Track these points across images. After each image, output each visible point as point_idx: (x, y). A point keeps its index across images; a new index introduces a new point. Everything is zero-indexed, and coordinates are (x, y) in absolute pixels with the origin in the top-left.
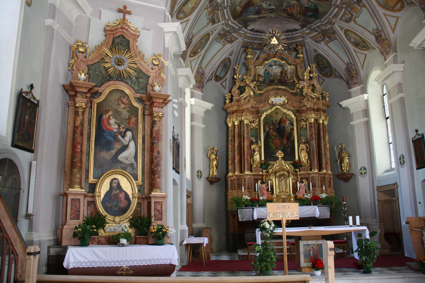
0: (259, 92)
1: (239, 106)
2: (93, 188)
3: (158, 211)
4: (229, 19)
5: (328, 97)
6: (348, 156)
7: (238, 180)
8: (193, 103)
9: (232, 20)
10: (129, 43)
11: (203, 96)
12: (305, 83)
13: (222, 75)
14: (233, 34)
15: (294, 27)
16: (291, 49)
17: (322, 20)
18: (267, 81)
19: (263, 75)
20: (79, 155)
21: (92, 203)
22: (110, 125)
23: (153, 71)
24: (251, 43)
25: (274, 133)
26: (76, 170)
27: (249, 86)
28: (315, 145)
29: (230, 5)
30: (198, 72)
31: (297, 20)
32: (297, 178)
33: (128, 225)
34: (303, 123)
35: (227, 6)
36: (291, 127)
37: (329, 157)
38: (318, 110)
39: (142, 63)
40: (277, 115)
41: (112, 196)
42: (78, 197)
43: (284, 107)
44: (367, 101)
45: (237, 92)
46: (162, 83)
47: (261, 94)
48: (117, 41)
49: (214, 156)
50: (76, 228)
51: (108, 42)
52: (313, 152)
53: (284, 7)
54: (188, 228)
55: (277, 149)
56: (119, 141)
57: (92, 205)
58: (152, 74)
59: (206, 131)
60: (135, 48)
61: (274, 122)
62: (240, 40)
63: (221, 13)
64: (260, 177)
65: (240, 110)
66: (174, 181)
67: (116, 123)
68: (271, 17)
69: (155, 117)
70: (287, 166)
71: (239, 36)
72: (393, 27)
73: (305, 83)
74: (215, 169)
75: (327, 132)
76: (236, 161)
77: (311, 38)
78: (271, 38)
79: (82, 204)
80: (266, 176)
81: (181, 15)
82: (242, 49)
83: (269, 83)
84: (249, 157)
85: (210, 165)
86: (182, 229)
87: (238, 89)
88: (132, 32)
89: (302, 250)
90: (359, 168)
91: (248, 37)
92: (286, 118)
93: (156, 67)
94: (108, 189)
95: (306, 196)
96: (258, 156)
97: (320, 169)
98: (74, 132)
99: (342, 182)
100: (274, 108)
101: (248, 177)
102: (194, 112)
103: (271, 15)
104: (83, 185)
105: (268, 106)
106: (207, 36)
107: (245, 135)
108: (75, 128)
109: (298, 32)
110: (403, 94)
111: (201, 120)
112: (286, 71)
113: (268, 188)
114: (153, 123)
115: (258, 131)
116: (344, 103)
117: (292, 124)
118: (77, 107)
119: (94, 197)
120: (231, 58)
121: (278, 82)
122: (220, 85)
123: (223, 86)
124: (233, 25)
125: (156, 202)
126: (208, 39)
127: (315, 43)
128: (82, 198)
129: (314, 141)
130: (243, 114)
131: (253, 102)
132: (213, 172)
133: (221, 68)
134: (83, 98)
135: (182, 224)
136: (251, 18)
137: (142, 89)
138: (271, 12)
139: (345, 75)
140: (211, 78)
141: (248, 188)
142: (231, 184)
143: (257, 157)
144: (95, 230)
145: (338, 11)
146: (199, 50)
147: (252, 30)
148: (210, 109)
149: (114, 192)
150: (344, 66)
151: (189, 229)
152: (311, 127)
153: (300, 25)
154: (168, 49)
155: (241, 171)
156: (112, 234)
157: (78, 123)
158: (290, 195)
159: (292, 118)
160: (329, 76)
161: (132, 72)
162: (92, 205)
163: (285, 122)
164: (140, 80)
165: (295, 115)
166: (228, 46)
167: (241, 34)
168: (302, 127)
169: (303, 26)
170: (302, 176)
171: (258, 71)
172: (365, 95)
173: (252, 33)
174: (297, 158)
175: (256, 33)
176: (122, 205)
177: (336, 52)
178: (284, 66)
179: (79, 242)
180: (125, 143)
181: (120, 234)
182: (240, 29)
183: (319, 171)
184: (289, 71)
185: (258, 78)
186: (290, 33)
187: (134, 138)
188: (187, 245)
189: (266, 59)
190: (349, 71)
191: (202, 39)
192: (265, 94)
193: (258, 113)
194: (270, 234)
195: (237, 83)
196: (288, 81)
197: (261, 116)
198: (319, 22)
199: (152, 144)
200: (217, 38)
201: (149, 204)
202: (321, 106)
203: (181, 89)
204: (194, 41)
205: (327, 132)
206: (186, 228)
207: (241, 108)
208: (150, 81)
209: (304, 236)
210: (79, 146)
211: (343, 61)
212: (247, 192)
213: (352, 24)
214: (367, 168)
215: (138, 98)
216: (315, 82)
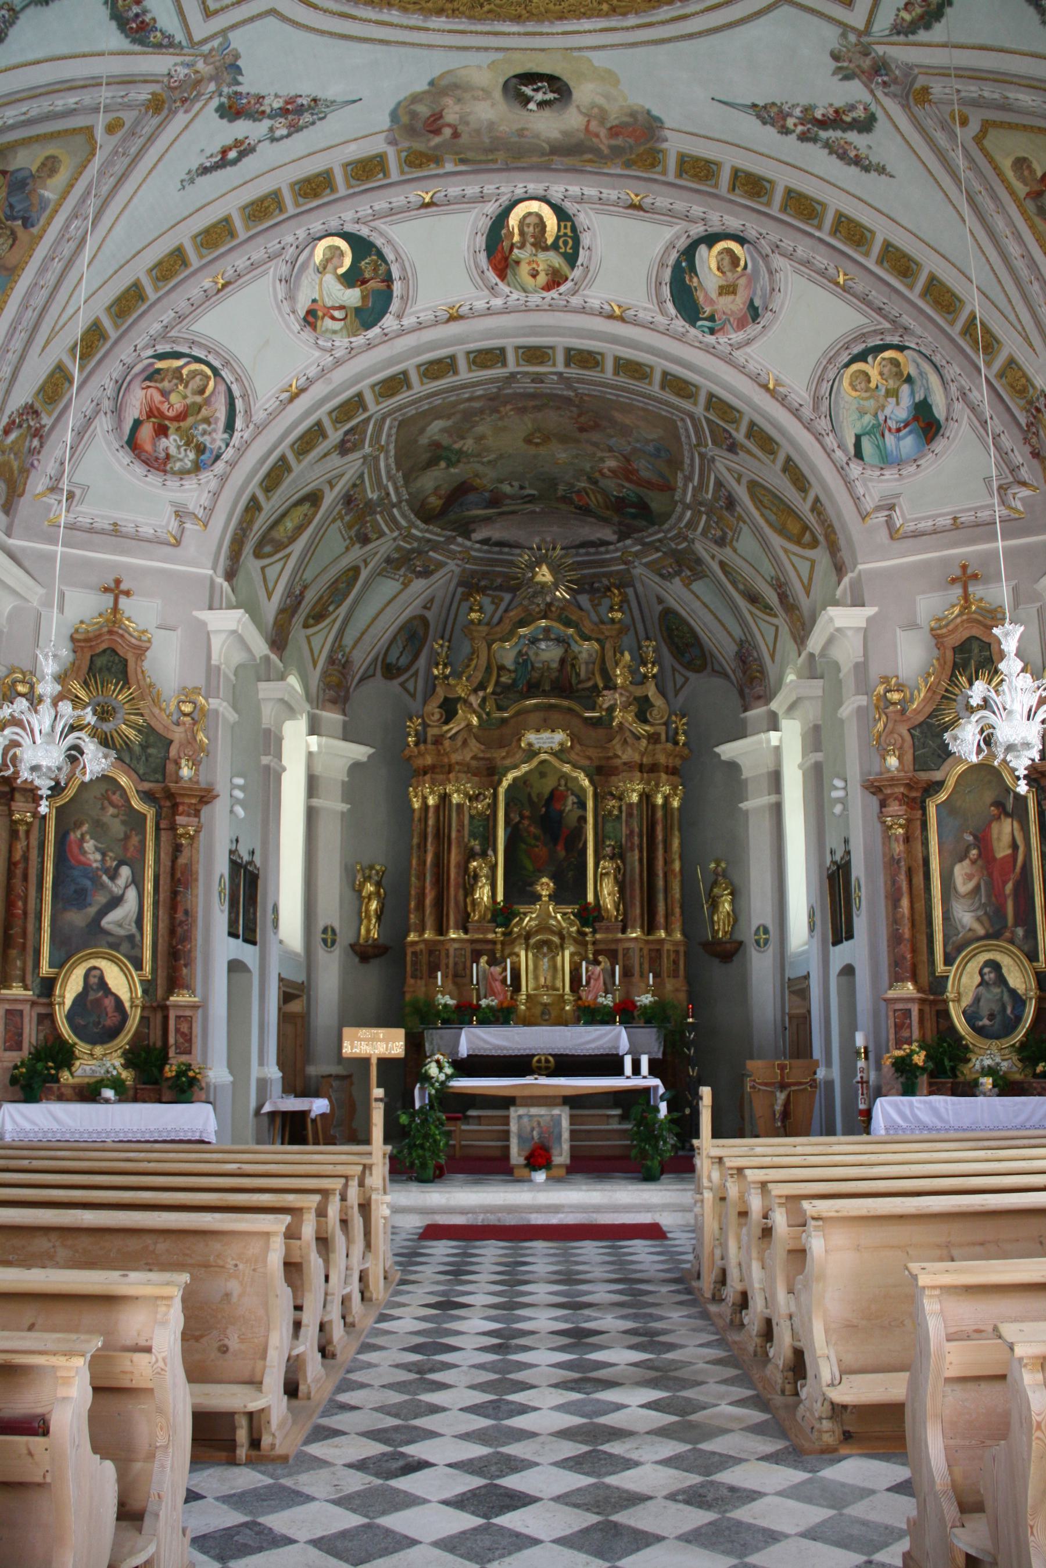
0: (497, 715)
1: (439, 753)
2: (48, 987)
3: (183, 1034)
4: (411, 525)
5: (685, 733)
6: (732, 894)
7: (431, 952)
8: (314, 748)
9: (422, 526)
10: (126, 666)
11: (345, 724)
12: (617, 696)
13: (403, 661)
14: (431, 553)
15: (599, 535)
16: (598, 590)
17: (666, 526)
18: (521, 685)
19: (512, 668)
20: (20, 922)
21: (47, 1018)
22: (84, 853)
23: (181, 729)
24: (485, 574)
25: (532, 829)
26: (14, 952)
27: (466, 701)
28: (637, 864)
29: (406, 497)
30: (331, 661)
31: (605, 521)
32: (586, 951)
33: (118, 1062)
34: (613, 802)
35: (400, 501)
36: (580, 812)
37: (677, 896)
38: (653, 768)
39: (156, 711)
40: (544, 780)
41: (88, 1004)
42: (19, 1007)
43: (564, 757)
44: (778, 750)
45: (437, 717)
46: (198, 754)
47: (504, 721)
48: (99, 662)
49: (370, 888)
50: (16, 1067)
51: (79, 668)
52: (632, 883)
53: (560, 493)
54: (280, 1074)
55: (539, 872)
56: (103, 886)
57: (47, 1022)
58: (178, 735)
59: (352, 822)
60: (140, 677)
61: (535, 799)
62: (452, 566)
63: (383, 517)
64: (490, 947)
65: (442, 766)
66: (235, 967)
67: (97, 849)
68: (533, 512)
69: (182, 836)
70: (559, 916)
71: (448, 557)
72: (806, 581)
73: (617, 696)
74: (374, 921)
75: (676, 828)
76: (428, 901)
77: (646, 565)
78: (531, 566)
79: (26, 1020)
80: (503, 943)
81: (268, 549)
82: (460, 590)
83: (528, 690)
84: (461, 893)
85: (360, 913)
86: (262, 1076)
87: (440, 707)
88: (133, 641)
89: (513, 1127)
90: (754, 928)
91: (475, 558)
92: (568, 789)
93: (188, 719)
94: (80, 989)
95: (600, 1000)
96: (487, 890)
97: (650, 927)
98: (10, 874)
99: (716, 962)
100: (535, 762)
101: (456, 945)
102: (318, 770)
103: (530, 507)
104: (29, 982)
105: (519, 755)
106: (351, 573)
107: (454, 835)
108: (11, 865)
109: (611, 547)
110: (820, 754)
111: (338, 791)
112: (575, 658)
113: (505, 977)
114: (177, 849)
115: (491, 824)
116: (728, 751)
117: (582, 805)
118: (16, 822)
119: (51, 1005)
120: (429, 615)
121: (553, 689)
122: (399, 689)
123: (407, 690)
124: (427, 535)
125: (178, 1017)
126: (356, 578)
127: (657, 579)
128: (26, 1008)
129: (636, 852)
130: (451, 776)
131: (474, 746)
132: (368, 931)
133: (400, 644)
134: (27, 802)
135: (261, 1063)
136: (477, 516)
137: (155, 771)
138: (530, 502)
139: (734, 671)
140: (370, 672)
141: (456, 975)
142: (414, 964)
143: (483, 893)
144: (53, 1072)
145: (692, 515)
146: (331, 608)
147: (485, 542)
148: (365, 759)
149: (92, 996)
150: (730, 649)
151: (283, 1078)
152: (630, 815)
153: (615, 533)
154: (218, 668)
155: (441, 930)
156: (87, 1080)
157: (18, 855)
158: (562, 996)
159: (583, 790)
160: (699, 670)
161: (131, 733)
162: (47, 1022)
163: (563, 798)
164: (151, 751)
165: (591, 781)
166: (419, 585)
167: (454, 552)
168: (610, 812)
169: (623, 536)
170: (602, 947)
171: (497, 656)
172: (772, 733)
173: (486, 547)
174: (590, 898)
175: (497, 549)
176: (109, 1022)
177: (712, 607)
178: (572, 643)
179: (21, 1095)
180: (117, 891)
181: (102, 1080)
182: (451, 540)
183: (649, 933)
184: (584, 656)
185: (499, 676)
186: (592, 550)
187: (137, 881)
188: (272, 1114)
189: (522, 623)
190: (744, 662)
191: (336, 581)
192: (513, 721)
193: (491, 773)
194: (437, 1090)
195: (438, 689)
196: (580, 686)
197: (500, 782)
198: (659, 532)
199: (174, 894)
200: (384, 570)
201: (166, 1019)
202: (662, 759)
203: (268, 732)
204: (310, 596)
205: (676, 828)
206: (274, 1073)
207: (446, 760)
208: (173, 752)
209: (523, 1097)
210: (20, 904)
211: (729, 632)
212: (450, 986)
213: (728, 550)
214: (771, 928)
215: (145, 792)
216: (651, 690)
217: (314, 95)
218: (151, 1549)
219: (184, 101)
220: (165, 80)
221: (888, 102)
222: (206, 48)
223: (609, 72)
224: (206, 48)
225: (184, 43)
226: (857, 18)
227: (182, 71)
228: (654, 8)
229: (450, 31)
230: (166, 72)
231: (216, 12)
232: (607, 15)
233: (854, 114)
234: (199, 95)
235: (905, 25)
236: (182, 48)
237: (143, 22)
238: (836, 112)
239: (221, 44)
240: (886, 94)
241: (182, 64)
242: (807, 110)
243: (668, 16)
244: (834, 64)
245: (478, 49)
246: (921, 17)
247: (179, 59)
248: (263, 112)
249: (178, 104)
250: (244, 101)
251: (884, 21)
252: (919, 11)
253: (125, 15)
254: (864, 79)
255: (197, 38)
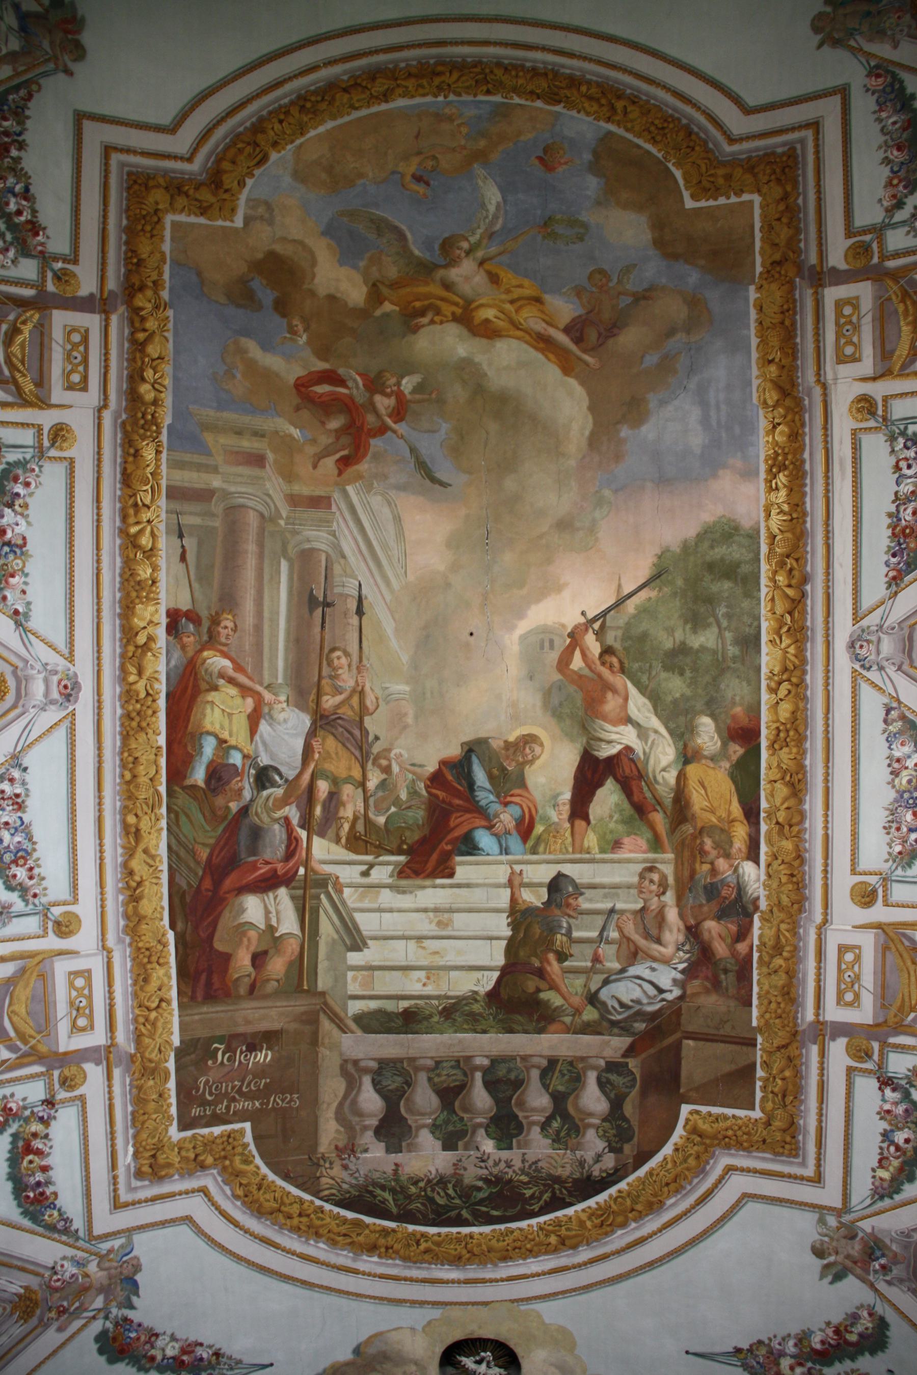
217: (217, 1346)
218: (209, 747)
219: (62, 1311)
220: (47, 1274)
221: (894, 1293)
222: (105, 1246)
223: (563, 1330)
224: (105, 1246)
225: (81, 1233)
226: (831, 1195)
227: (70, 1269)
228: (606, 1234)
229: (382, 1277)
230: (51, 1265)
231: (126, 1205)
232: (556, 1250)
233: (859, 1328)
234: (82, 1309)
235: (886, 1185)
236: (78, 1239)
237: (42, 1194)
238: (837, 1331)
239: (122, 1246)
240: (889, 1283)
241: (72, 1259)
242: (803, 1338)
243: (623, 1243)
244: (818, 1263)
245: (414, 1303)
246: (901, 1169)
247: (70, 1252)
248: (153, 1358)
249: (53, 1314)
250: (133, 1335)
251: (862, 1188)
252: (896, 1163)
253: (26, 1179)
254: (858, 1271)
255: (97, 1231)
